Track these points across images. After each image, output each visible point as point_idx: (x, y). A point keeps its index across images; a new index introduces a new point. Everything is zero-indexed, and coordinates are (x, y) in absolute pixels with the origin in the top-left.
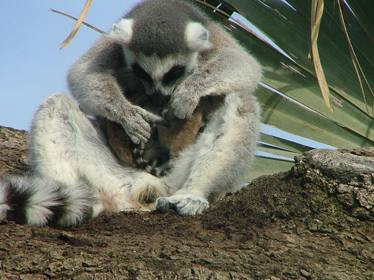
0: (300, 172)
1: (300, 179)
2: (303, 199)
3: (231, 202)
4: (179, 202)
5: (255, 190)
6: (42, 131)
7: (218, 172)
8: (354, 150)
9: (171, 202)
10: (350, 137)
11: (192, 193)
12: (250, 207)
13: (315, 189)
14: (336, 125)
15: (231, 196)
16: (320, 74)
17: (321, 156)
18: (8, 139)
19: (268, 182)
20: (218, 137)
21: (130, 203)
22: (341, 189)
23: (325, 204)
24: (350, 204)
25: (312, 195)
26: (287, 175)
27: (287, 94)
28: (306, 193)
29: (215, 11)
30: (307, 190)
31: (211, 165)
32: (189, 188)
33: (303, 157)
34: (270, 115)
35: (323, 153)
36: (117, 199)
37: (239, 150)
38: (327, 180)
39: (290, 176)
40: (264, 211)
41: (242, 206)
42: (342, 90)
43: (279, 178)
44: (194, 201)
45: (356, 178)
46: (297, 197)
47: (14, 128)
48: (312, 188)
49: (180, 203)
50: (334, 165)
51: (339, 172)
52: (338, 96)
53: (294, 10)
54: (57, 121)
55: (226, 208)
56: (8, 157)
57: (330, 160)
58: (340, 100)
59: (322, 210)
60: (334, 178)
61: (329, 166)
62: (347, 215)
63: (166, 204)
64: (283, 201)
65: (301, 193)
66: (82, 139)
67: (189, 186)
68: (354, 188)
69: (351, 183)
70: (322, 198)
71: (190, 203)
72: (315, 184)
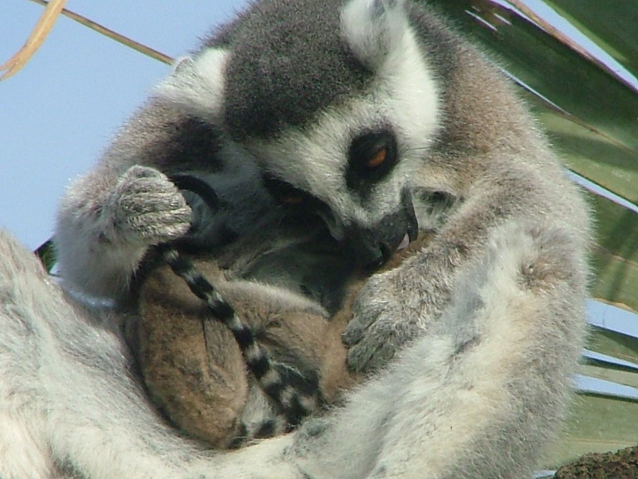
7: (462, 450)
20: (462, 348)
34: (620, 275)
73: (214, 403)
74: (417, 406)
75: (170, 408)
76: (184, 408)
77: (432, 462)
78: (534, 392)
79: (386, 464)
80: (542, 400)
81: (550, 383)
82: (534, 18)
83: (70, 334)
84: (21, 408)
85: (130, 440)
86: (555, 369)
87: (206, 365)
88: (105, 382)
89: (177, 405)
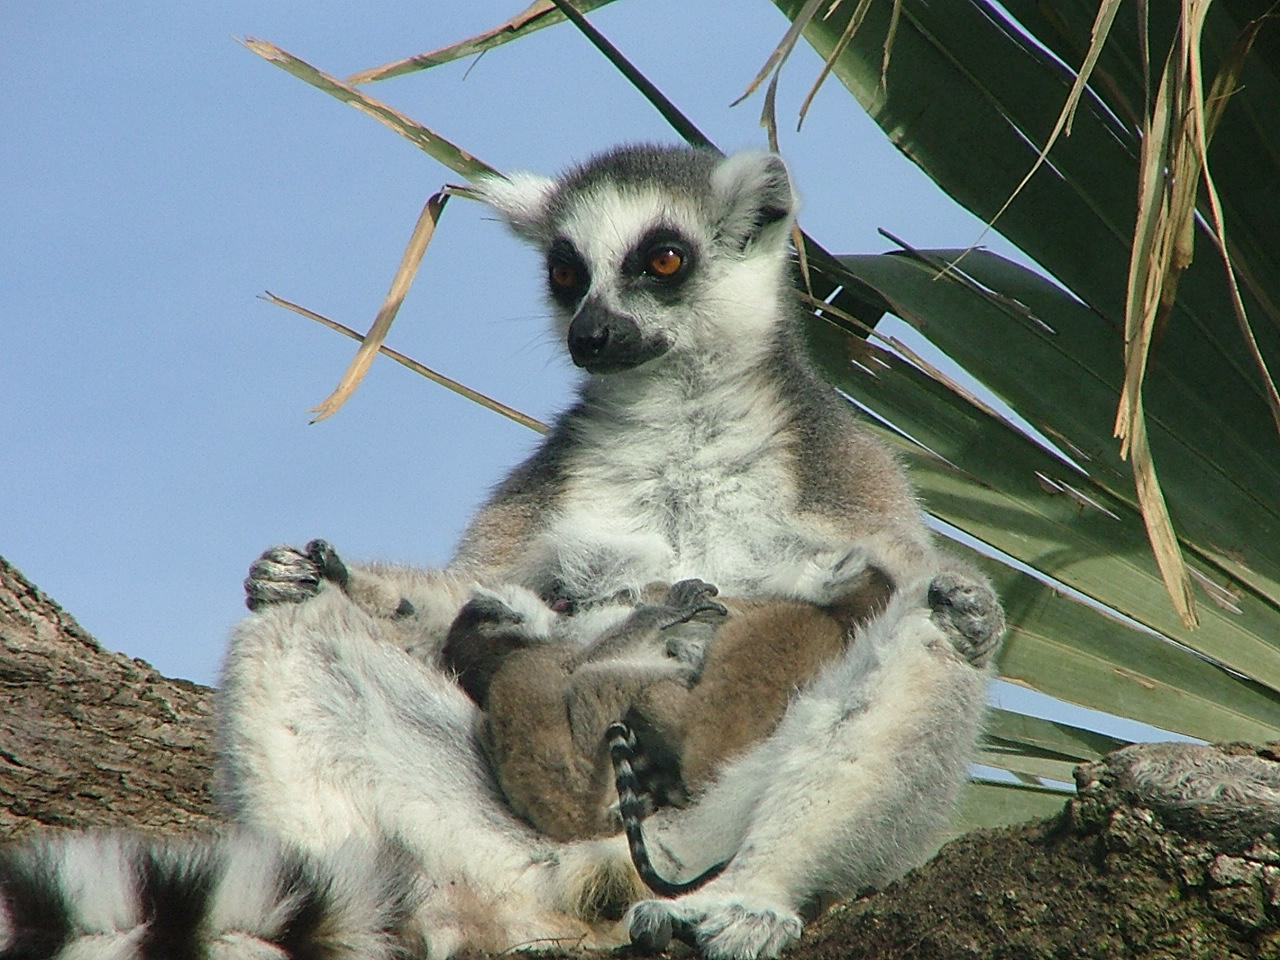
0: (1091, 819)
1: (1092, 840)
2: (1101, 907)
3: (869, 916)
4: (704, 918)
5: (948, 876)
7: (841, 829)
8: (1269, 744)
9: (677, 915)
11: (752, 888)
12: (928, 933)
13: (1138, 872)
14: (1221, 673)
15: (874, 897)
16: (1152, 505)
19: (990, 852)
20: (848, 715)
21: (550, 921)
22: (1223, 873)
23: (1171, 922)
24: (1251, 921)
25: (1127, 894)
26: (1052, 826)
27: (1059, 577)
28: (1110, 885)
29: (818, 313)
30: (1114, 877)
31: (818, 803)
32: (742, 872)
33: (1104, 768)
35: (1166, 754)
36: (507, 911)
37: (912, 760)
38: (1179, 844)
39: (1060, 830)
40: (974, 947)
41: (904, 929)
42: (1239, 559)
44: (752, 915)
45: (1270, 836)
46: (1080, 898)
48: (1128, 869)
49: (707, 922)
50: (1199, 793)
51: (1216, 817)
52: (1225, 580)
53: (1080, 304)
54: (301, 662)
55: (853, 938)
56: (168, 778)
57: (1188, 780)
58: (1231, 592)
59: (1159, 942)
60: (1200, 838)
61: (1184, 796)
62: (1241, 955)
63: (662, 925)
64: (1034, 914)
65: (1094, 884)
66: (388, 722)
67: (744, 867)
68: (1266, 869)
69: (1255, 852)
70: (1160, 900)
71: (741, 921)
72: (1138, 855)
74: (792, 777)
75: (533, 813)
76: (550, 811)
77: (806, 841)
78: (924, 770)
79: (754, 842)
80: (933, 778)
81: (942, 761)
83: (407, 699)
84: (346, 777)
85: (470, 816)
86: (949, 746)
87: (571, 757)
88: (445, 753)
89: (543, 807)
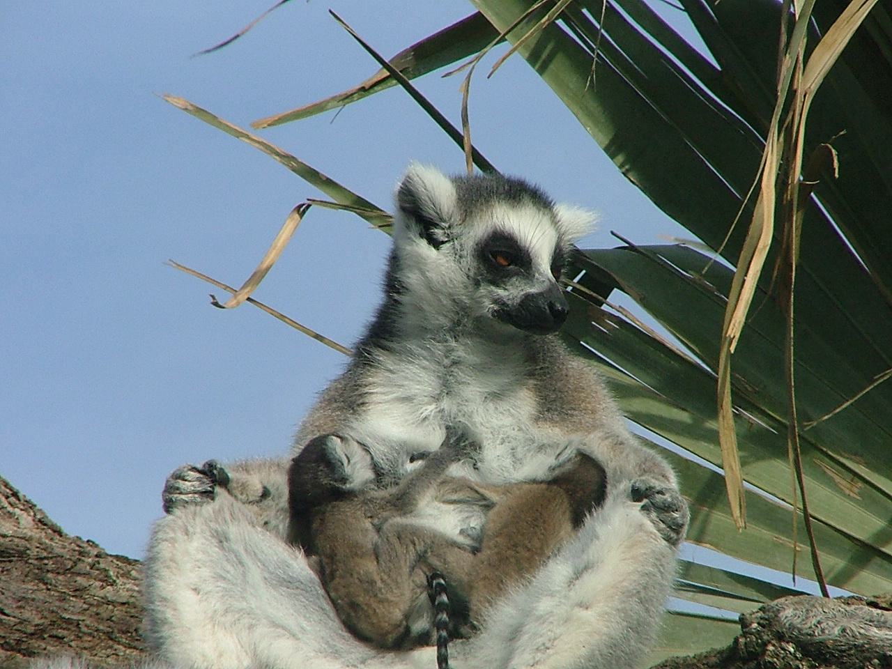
6: (168, 567)
8: (875, 597)
10: (881, 566)
17: (798, 612)
18: (115, 581)
34: (705, 522)
43: (707, 664)
45: (876, 661)
47: (130, 558)
50: (827, 632)
57: (819, 622)
61: (816, 634)
73: (386, 604)
76: (363, 609)
81: (647, 610)
82: (638, 323)
